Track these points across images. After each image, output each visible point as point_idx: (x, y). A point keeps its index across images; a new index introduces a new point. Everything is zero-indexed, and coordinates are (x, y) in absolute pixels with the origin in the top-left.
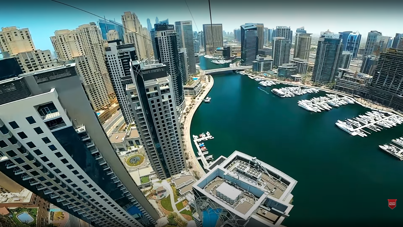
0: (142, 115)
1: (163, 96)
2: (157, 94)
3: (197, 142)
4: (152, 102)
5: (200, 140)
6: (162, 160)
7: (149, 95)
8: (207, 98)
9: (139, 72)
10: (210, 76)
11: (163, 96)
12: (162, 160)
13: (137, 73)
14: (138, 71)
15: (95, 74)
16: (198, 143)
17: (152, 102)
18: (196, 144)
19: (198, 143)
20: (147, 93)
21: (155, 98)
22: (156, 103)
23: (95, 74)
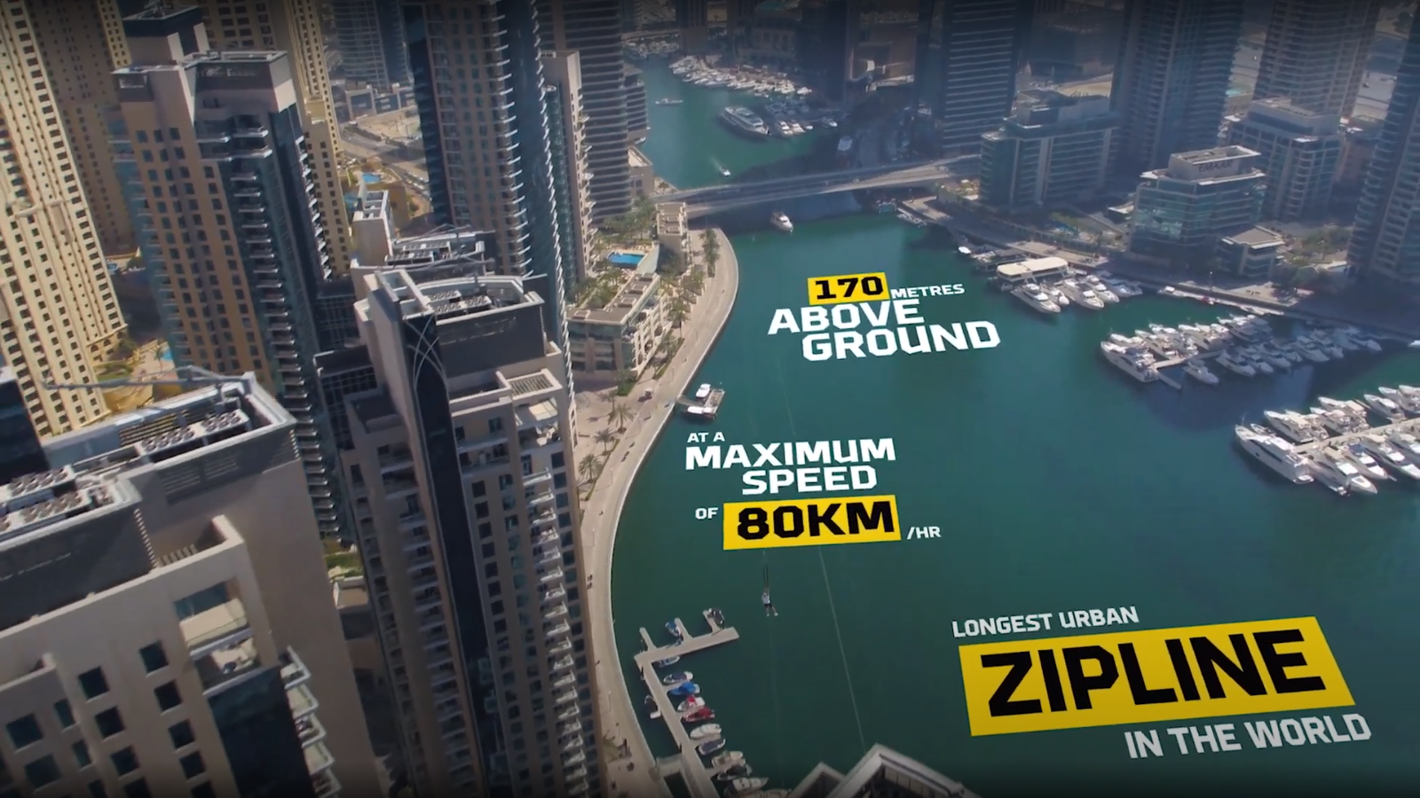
0: (429, 573)
1: (528, 457)
2: (500, 452)
3: (655, 665)
4: (479, 489)
5: (671, 653)
6: (925, 294)
7: (464, 457)
8: (704, 390)
9: (430, 354)
10: (720, 236)
11: (528, 457)
12: (925, 294)
13: (420, 357)
14: (423, 347)
15: (12, 218)
16: (661, 669)
17: (479, 489)
18: (651, 678)
19: (661, 669)
20: (460, 450)
21: (490, 475)
22: (493, 497)
23: (12, 218)
